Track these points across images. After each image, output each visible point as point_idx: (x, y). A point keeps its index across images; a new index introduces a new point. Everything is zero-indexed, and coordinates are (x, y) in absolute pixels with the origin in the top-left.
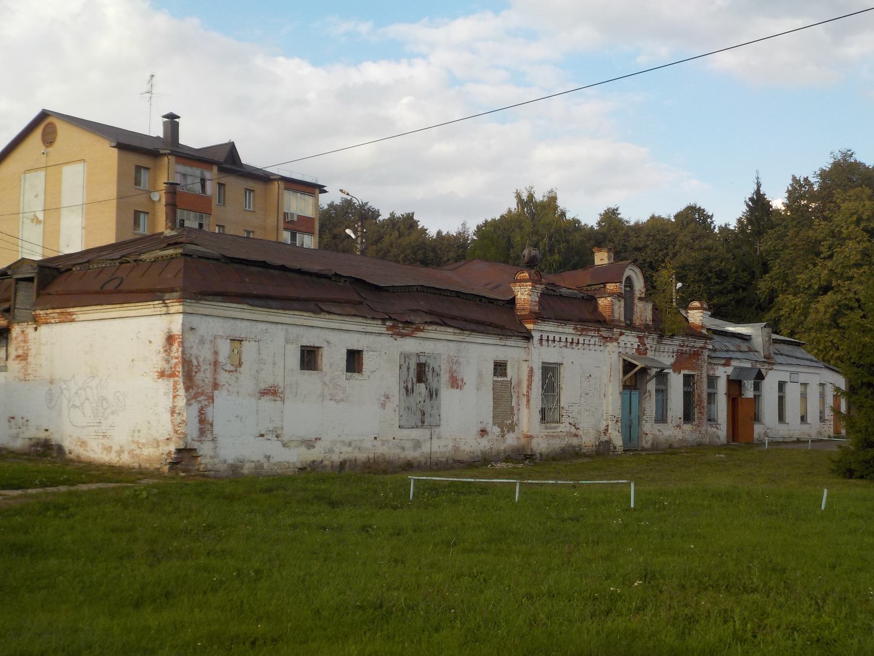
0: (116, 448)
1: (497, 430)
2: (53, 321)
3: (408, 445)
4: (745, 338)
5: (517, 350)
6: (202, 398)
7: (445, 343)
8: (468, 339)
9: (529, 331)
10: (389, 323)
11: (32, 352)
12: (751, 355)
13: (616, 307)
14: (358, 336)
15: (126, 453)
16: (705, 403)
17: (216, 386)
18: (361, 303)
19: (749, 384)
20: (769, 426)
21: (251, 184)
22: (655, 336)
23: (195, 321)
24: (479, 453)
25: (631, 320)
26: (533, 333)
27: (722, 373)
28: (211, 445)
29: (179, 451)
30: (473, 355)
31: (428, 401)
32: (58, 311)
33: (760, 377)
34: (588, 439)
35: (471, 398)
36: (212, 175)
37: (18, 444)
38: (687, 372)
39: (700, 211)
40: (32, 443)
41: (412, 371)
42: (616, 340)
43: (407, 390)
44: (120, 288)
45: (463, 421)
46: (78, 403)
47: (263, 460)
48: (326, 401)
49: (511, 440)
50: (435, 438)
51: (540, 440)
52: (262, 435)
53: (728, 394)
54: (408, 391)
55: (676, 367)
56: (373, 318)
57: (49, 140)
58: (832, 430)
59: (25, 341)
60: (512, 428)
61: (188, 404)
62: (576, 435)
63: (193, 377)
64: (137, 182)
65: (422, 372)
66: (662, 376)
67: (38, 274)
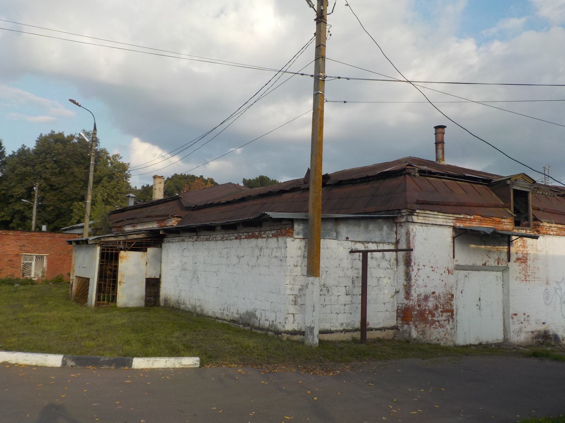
2: (552, 233)
32: (560, 226)
40: (534, 335)
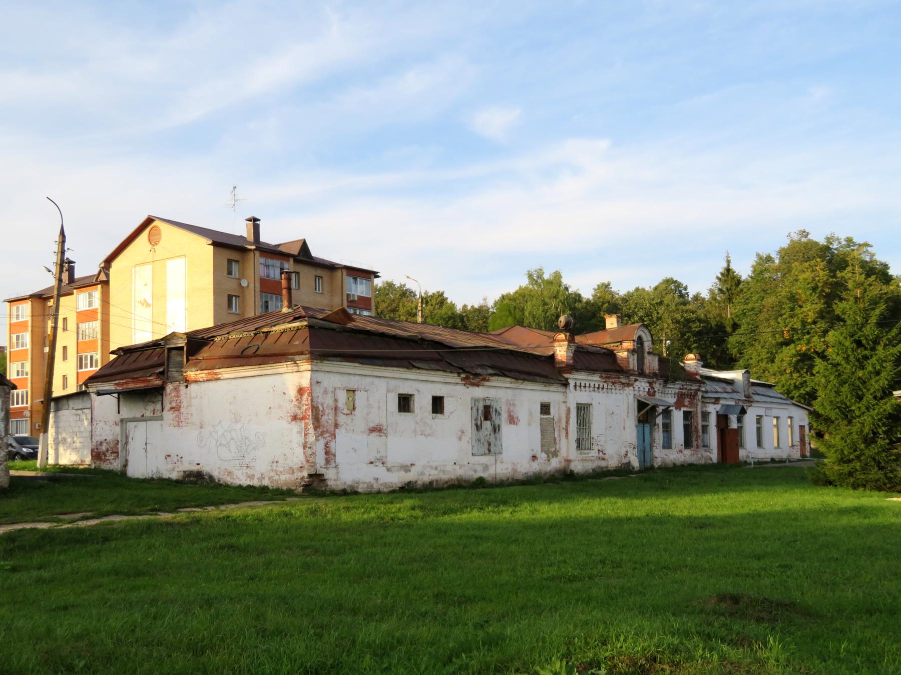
0: (258, 475)
1: (544, 455)
3: (479, 468)
4: (730, 382)
5: (557, 394)
6: (327, 435)
7: (504, 390)
8: (521, 386)
9: (567, 379)
10: (463, 376)
11: (184, 404)
12: (735, 396)
13: (631, 360)
14: (440, 386)
15: (267, 479)
16: (700, 431)
17: (336, 426)
18: (441, 360)
19: (733, 418)
20: (749, 450)
21: (319, 272)
22: (661, 381)
23: (320, 376)
24: (531, 474)
25: (642, 370)
26: (570, 381)
27: (713, 410)
28: (334, 471)
29: (310, 476)
30: (521, 399)
31: (492, 435)
33: (743, 412)
34: (613, 463)
35: (526, 431)
36: (289, 266)
37: (174, 476)
38: (685, 409)
39: (678, 285)
41: (480, 411)
42: (632, 385)
43: (477, 427)
44: (258, 353)
45: (519, 450)
46: (224, 442)
47: (373, 482)
48: (409, 437)
49: (555, 464)
50: (498, 462)
51: (577, 463)
52: (372, 463)
53: (718, 425)
54: (478, 427)
55: (678, 405)
56: (451, 372)
57: (154, 241)
58: (799, 453)
59: (178, 396)
60: (555, 454)
61: (317, 440)
62: (603, 459)
63: (317, 417)
64: (230, 273)
65: (487, 412)
66: (667, 413)
67: (187, 344)
